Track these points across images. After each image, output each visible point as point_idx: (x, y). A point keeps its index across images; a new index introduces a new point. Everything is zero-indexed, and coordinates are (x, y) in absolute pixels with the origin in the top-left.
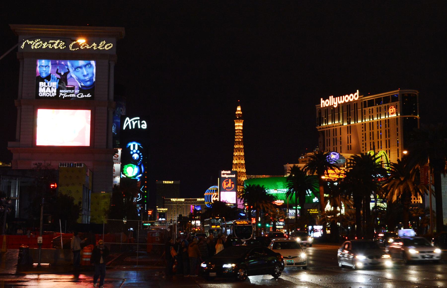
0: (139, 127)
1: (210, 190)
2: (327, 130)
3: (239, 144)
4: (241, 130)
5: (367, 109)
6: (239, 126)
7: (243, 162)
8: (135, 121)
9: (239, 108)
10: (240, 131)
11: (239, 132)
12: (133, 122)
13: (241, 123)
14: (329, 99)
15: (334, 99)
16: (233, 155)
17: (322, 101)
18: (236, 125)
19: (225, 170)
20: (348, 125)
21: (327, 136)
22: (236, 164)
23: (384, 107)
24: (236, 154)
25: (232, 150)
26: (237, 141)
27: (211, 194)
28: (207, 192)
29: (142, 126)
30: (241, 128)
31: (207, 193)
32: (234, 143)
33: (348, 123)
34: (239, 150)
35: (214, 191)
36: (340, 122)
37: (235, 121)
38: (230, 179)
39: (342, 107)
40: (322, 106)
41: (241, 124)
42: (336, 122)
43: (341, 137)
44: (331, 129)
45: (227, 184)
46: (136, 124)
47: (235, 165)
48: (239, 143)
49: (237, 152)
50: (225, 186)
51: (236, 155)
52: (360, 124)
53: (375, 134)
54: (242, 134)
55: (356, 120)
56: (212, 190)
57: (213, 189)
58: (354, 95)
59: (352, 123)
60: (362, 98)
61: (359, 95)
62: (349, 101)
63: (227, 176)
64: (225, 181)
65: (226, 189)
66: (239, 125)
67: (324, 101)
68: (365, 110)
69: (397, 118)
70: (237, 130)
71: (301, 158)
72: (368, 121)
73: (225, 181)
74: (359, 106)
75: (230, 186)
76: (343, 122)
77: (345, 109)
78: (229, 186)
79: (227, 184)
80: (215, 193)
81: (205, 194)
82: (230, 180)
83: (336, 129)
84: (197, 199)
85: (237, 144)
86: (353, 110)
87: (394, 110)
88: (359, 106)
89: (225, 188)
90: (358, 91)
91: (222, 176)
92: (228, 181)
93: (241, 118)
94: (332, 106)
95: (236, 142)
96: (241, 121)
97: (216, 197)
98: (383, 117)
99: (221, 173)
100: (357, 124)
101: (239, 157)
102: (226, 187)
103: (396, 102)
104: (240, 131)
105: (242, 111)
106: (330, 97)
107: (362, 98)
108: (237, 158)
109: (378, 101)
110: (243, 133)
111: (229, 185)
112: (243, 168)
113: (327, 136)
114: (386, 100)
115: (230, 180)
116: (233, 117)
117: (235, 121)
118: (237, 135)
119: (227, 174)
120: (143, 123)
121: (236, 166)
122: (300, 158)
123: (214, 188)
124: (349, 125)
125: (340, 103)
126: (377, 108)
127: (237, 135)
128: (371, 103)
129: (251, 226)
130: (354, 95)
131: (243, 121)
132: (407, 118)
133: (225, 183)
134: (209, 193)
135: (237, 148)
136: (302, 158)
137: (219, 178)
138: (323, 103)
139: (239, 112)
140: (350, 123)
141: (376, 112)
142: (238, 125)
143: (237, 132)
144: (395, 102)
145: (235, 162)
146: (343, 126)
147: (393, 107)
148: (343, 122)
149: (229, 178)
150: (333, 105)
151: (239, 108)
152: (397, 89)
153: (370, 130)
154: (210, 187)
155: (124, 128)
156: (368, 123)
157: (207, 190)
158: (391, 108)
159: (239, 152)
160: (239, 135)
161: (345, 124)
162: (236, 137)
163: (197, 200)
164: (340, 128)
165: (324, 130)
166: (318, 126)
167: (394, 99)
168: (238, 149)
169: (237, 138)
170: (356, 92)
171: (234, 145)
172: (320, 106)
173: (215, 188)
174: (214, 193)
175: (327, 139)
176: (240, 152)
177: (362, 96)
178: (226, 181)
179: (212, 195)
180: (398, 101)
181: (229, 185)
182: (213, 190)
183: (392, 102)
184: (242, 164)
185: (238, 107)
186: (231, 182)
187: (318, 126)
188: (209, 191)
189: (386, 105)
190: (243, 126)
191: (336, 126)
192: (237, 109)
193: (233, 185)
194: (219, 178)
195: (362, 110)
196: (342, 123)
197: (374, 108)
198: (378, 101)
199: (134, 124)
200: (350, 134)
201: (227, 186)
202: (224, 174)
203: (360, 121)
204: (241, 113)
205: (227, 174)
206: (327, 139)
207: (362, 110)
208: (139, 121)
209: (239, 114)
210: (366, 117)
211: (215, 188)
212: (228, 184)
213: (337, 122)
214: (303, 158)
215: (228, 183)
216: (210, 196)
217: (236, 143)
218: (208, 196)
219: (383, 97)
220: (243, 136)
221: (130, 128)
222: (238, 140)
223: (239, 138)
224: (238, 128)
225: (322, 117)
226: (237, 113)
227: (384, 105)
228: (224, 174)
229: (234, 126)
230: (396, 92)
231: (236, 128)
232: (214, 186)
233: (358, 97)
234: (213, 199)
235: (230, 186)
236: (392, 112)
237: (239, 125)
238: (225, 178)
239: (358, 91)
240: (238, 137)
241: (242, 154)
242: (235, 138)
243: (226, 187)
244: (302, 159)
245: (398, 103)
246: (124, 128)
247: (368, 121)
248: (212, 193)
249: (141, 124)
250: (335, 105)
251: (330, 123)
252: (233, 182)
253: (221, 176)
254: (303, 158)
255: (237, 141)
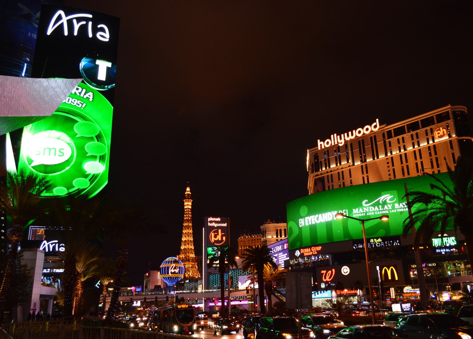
0: (90, 35)
1: (167, 261)
2: (328, 176)
3: (188, 222)
4: (189, 209)
5: (394, 140)
6: (188, 205)
7: (191, 239)
8: (79, 20)
9: (188, 189)
10: (189, 210)
11: (188, 211)
12: (75, 21)
13: (190, 202)
14: (212, 223)
15: (338, 137)
16: (182, 233)
17: (319, 143)
18: (185, 204)
19: (213, 217)
20: (362, 165)
21: (328, 182)
22: (185, 241)
23: (425, 132)
24: (184, 231)
25: (181, 228)
26: (186, 219)
27: (168, 265)
28: (164, 263)
29: (99, 35)
30: (190, 207)
31: (164, 264)
32: (182, 221)
33: (361, 161)
34: (188, 227)
35: (172, 263)
36: (350, 161)
37: (184, 200)
38: (220, 229)
39: (351, 144)
40: (319, 149)
41: (190, 204)
42: (343, 163)
43: (351, 180)
44: (335, 173)
45: (215, 237)
46: (54, 247)
47: (184, 243)
48: (188, 221)
49: (186, 229)
50: (213, 239)
51: (184, 232)
52: (382, 160)
53: (412, 167)
54: (191, 213)
55: (375, 154)
56: (169, 261)
57: (171, 260)
58: (363, 129)
59: (369, 160)
60: (384, 127)
61: (380, 125)
62: (224, 226)
63: (216, 225)
64: (212, 232)
65: (214, 243)
66: (188, 205)
67: (322, 143)
68: (390, 142)
69: (429, 147)
70: (187, 208)
71: (241, 238)
72: (396, 153)
73: (212, 232)
74: (379, 138)
75: (220, 239)
76: (353, 162)
77: (356, 146)
78: (218, 239)
79: (215, 237)
80: (173, 264)
81: (161, 266)
82: (220, 231)
83: (342, 172)
84: (127, 288)
85: (186, 222)
86: (370, 145)
87: (443, 132)
88: (379, 138)
89: (213, 241)
90: (377, 120)
91: (209, 224)
92: (218, 232)
93: (189, 197)
94: (335, 145)
95: (185, 220)
96: (191, 201)
97: (174, 269)
98: (424, 144)
99: (208, 220)
100: (378, 160)
101: (188, 234)
102: (214, 240)
103: (447, 122)
104: (189, 210)
105: (191, 191)
106: (332, 136)
107: (384, 127)
108: (186, 235)
109: (413, 127)
110: (191, 212)
111: (219, 237)
112: (192, 245)
113: (328, 182)
114: (427, 122)
115: (220, 231)
116: (183, 197)
117: (184, 200)
118: (186, 214)
119: (216, 222)
120: (102, 30)
121: (185, 243)
122: (240, 238)
123: (172, 259)
124: (364, 164)
125: (347, 139)
126: (412, 135)
127: (186, 214)
128: (399, 131)
129: (426, 284)
130: (363, 129)
131: (192, 200)
132: (464, 141)
133: (213, 235)
134: (166, 265)
135: (186, 226)
136: (241, 238)
137: (204, 228)
138: (321, 145)
139: (188, 193)
140: (365, 161)
141: (411, 139)
142: (187, 204)
143: (186, 211)
144: (443, 121)
145: (184, 239)
146: (353, 167)
147: (441, 128)
148: (353, 162)
149: (218, 228)
150: (337, 144)
151: (188, 189)
152: (448, 105)
153: (402, 163)
154: (166, 259)
155: (49, 32)
156: (396, 156)
157: (164, 262)
158: (437, 131)
159: (188, 229)
160: (188, 213)
161: (358, 163)
162: (185, 216)
163: (128, 289)
164: (342, 172)
165: (322, 177)
166: (314, 172)
167: (441, 118)
168: (187, 227)
169: (186, 216)
170: (376, 122)
171: (183, 223)
172: (318, 149)
173: (173, 259)
174: (172, 264)
175: (329, 187)
176: (189, 229)
177: (383, 126)
178: (214, 232)
179: (170, 267)
180: (450, 119)
181: (219, 237)
182: (171, 261)
183: (438, 122)
184: (191, 241)
185: (188, 188)
186: (221, 233)
187: (314, 172)
188: (166, 263)
189: (428, 128)
190: (192, 206)
191: (342, 168)
192: (186, 190)
193: (224, 238)
194: (204, 228)
195: (385, 142)
196: (352, 163)
197: (407, 136)
198: (413, 127)
199: (77, 27)
200: (367, 175)
201: (216, 239)
202: (211, 222)
203: (382, 156)
204: (190, 193)
205: (216, 222)
206: (329, 187)
207: (385, 142)
208: (90, 23)
209: (188, 194)
210: (392, 150)
211: (173, 259)
212: (217, 236)
213: (344, 163)
214: (242, 238)
215: (218, 235)
216: (168, 268)
217: (185, 221)
218: (165, 268)
219: (421, 120)
220: (192, 214)
221: (66, 33)
222: (187, 219)
223: (188, 216)
224: (188, 207)
225: (320, 161)
226: (186, 193)
227: (424, 129)
228: (211, 222)
229: (184, 206)
230: (447, 108)
231: (185, 207)
232: (171, 257)
233: (378, 127)
234: (171, 271)
235: (220, 239)
236: (439, 135)
237: (188, 205)
238: (213, 227)
239: (377, 120)
240: (187, 215)
241: (191, 231)
242: (184, 216)
243: (214, 240)
244: (241, 239)
245: (451, 122)
246: (49, 32)
247: (396, 153)
248: (170, 264)
249: (95, 30)
250: (341, 143)
251: (333, 166)
252: (223, 234)
253: (208, 224)
254: (242, 238)
255: (186, 219)
